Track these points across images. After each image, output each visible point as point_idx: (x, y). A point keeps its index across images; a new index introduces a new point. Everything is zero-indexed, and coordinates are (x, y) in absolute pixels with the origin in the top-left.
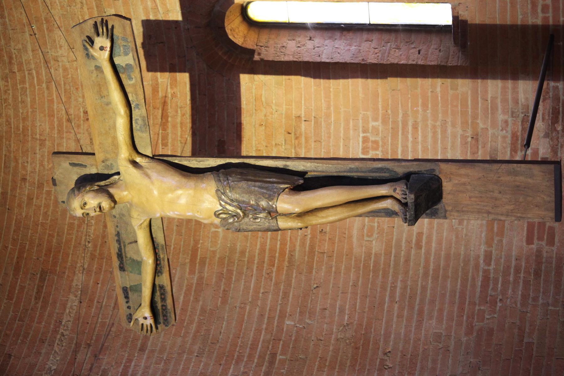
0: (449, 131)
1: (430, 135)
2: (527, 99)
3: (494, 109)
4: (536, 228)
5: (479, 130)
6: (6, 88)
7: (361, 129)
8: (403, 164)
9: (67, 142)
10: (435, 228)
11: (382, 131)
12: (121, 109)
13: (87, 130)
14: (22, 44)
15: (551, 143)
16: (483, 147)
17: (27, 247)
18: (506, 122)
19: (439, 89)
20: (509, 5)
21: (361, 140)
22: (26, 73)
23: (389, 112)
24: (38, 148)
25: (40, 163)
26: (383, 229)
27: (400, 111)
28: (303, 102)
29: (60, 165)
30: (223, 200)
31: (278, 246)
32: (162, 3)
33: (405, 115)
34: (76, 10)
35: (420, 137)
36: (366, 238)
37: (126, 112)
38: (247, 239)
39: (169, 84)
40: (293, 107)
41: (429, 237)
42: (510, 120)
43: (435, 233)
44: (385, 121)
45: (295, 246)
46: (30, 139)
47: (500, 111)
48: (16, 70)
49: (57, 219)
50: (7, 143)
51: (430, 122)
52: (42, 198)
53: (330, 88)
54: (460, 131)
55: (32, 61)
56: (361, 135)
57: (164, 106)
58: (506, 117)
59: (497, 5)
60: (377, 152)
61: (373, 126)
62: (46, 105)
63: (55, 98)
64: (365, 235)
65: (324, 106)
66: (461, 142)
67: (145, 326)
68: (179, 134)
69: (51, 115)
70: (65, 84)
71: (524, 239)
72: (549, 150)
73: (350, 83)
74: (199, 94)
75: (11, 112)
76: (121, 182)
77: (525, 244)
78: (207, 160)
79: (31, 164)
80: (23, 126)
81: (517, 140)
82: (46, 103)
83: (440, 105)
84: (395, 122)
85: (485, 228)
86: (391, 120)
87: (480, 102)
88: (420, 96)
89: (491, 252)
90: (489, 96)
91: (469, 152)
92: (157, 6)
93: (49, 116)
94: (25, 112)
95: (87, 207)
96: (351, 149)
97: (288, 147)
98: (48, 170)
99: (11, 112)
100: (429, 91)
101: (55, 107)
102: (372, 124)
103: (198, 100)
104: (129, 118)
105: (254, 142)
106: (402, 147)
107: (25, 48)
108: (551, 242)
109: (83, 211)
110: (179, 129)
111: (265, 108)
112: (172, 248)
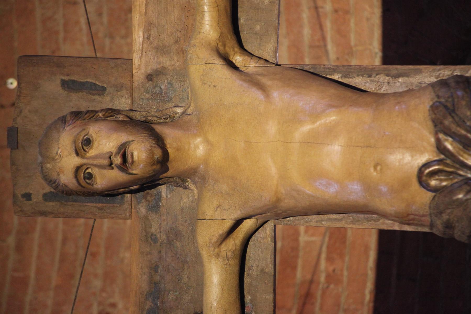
30: (448, 133)
39: (324, 249)
57: (304, 304)
70: (65, 240)
76: (187, 118)
92: (324, 38)
95: (92, 153)
109: (77, 161)
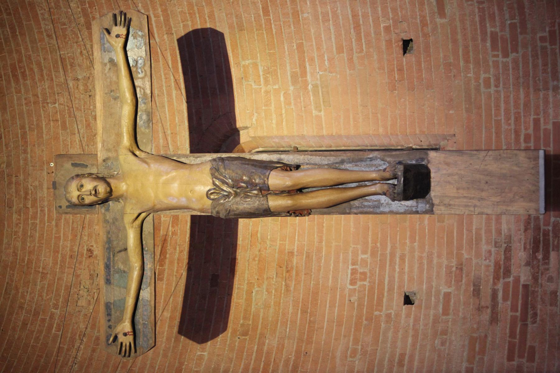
0: (435, 261)
1: (416, 266)
2: (509, 230)
3: (478, 239)
4: (517, 347)
5: (464, 260)
6: (18, 221)
7: (350, 262)
8: (394, 153)
9: (67, 276)
10: (418, 350)
11: (370, 263)
12: (128, 96)
13: (88, 266)
14: (39, 181)
15: (532, 271)
16: (467, 276)
17: (15, 364)
18: (490, 252)
19: (426, 222)
20: (494, 134)
21: (349, 271)
22: (39, 209)
23: (379, 245)
24: (39, 280)
25: (39, 294)
26: (367, 351)
27: (389, 244)
28: (296, 237)
29: (62, 166)
30: (217, 178)
31: (262, 366)
32: (173, 141)
33: (393, 248)
34: (93, 150)
35: (406, 268)
36: (349, 359)
37: (132, 100)
38: (232, 361)
40: (287, 242)
41: (412, 357)
42: (493, 250)
43: (417, 354)
44: (374, 254)
45: (278, 366)
46: (33, 271)
47: (484, 241)
48: (29, 206)
49: (48, 343)
50: (11, 272)
51: (417, 254)
52: (36, 324)
53: (323, 223)
54: (445, 262)
55: (45, 199)
56: (350, 267)
58: (489, 247)
59: (483, 136)
60: (365, 283)
61: (362, 258)
62: (53, 241)
63: (62, 235)
64: (348, 356)
65: (316, 239)
66: (446, 271)
67: (124, 344)
68: (175, 270)
69: (56, 252)
70: (73, 222)
71: (505, 357)
72: (530, 278)
73: (343, 218)
74: (198, 232)
75: (19, 244)
76: (119, 175)
77: (505, 361)
78: (205, 156)
79: (30, 294)
80: (28, 259)
81: (500, 268)
82: (53, 239)
83: (427, 237)
84: (383, 255)
85: (467, 348)
86: (379, 252)
87: (465, 233)
88: (408, 229)
89: (472, 368)
90: (474, 228)
91: (453, 280)
92: (168, 144)
93: (54, 252)
94: (32, 246)
95: (84, 190)
96: (339, 280)
97: (280, 280)
98: (45, 300)
99: (19, 244)
100: (417, 224)
101: (61, 244)
102: (361, 256)
103: (197, 237)
104: (135, 108)
105: (246, 276)
106: (389, 277)
107: (41, 185)
108: (531, 359)
110: (176, 264)
111: (260, 244)
112: (156, 369)
